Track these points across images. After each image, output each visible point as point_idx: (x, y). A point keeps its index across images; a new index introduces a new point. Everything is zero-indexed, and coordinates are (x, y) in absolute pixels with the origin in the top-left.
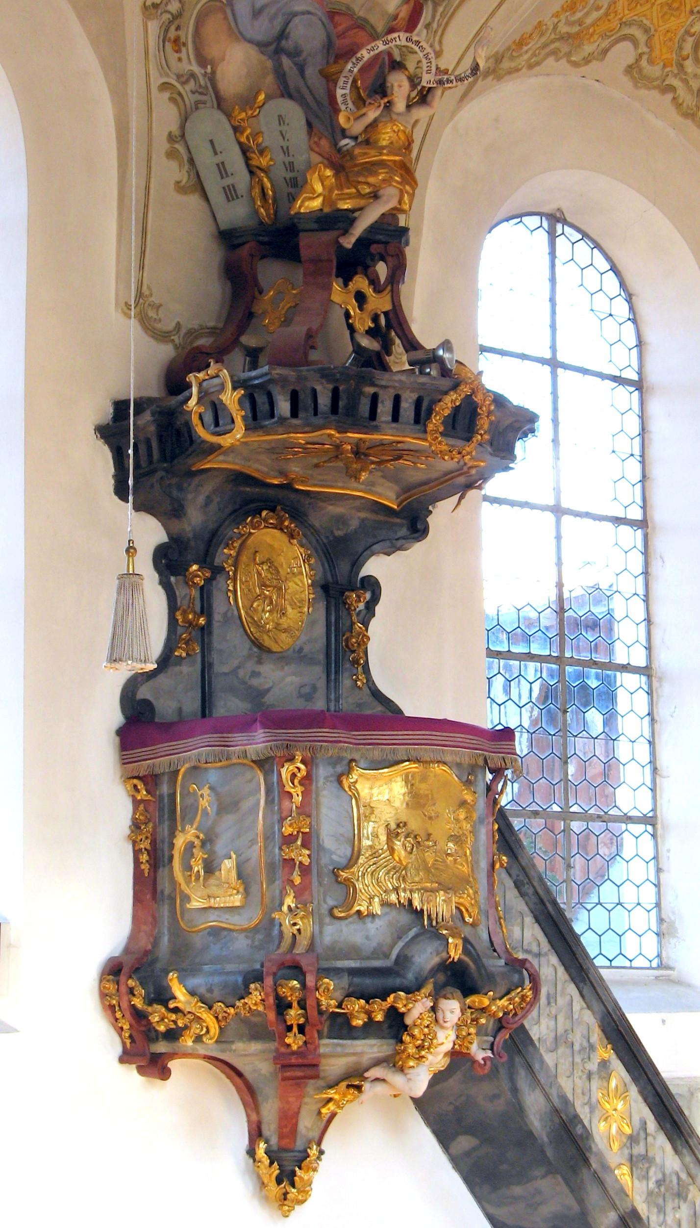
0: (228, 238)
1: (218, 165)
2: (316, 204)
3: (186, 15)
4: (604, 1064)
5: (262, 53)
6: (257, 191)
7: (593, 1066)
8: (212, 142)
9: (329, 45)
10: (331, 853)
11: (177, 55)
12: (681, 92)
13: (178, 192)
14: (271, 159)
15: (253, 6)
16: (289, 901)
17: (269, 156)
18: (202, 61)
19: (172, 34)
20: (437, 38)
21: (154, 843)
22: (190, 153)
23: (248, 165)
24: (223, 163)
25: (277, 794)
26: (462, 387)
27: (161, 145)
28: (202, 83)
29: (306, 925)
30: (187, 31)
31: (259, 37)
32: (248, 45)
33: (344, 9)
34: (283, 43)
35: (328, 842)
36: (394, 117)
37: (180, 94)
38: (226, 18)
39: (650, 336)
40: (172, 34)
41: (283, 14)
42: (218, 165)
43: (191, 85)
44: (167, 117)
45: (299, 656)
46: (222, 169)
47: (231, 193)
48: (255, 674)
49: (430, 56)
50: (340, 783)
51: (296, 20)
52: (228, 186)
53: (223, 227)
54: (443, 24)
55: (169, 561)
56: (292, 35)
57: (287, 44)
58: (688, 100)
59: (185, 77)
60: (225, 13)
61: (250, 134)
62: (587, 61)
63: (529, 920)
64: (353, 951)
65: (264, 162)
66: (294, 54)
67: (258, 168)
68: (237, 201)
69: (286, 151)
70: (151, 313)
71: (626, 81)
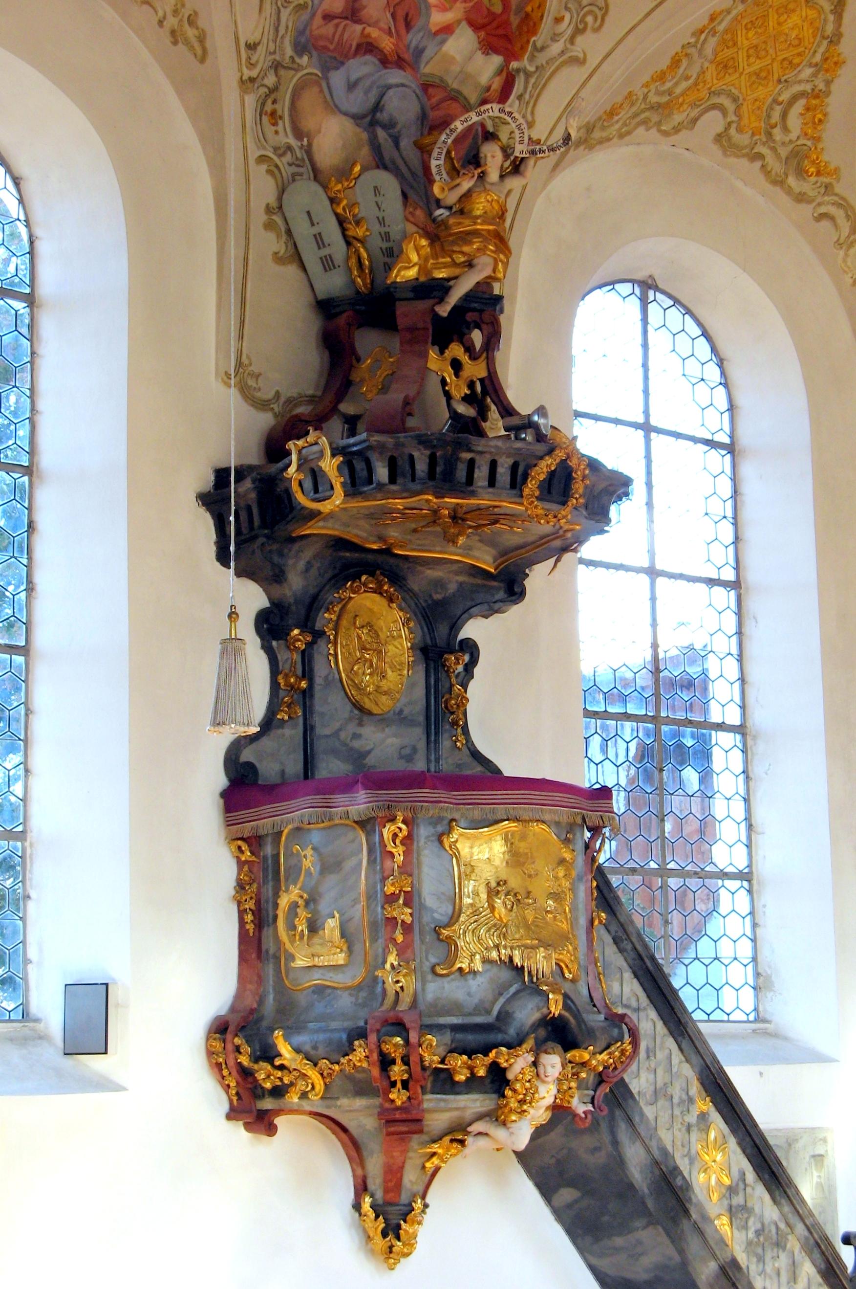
0: (325, 307)
1: (315, 236)
2: (412, 273)
3: (282, 88)
4: (703, 1116)
5: (357, 125)
6: (353, 262)
7: (692, 1118)
8: (308, 213)
9: (423, 117)
10: (432, 911)
11: (274, 128)
12: (770, 159)
14: (367, 230)
16: (392, 959)
18: (298, 133)
19: (269, 107)
20: (529, 109)
21: (258, 903)
22: (287, 224)
23: (345, 236)
24: (320, 234)
25: (379, 853)
27: (259, 217)
28: (299, 155)
29: (409, 983)
30: (284, 104)
31: (354, 110)
32: (344, 118)
33: (437, 81)
34: (378, 114)
35: (430, 901)
37: (277, 166)
38: (321, 91)
39: (741, 400)
40: (269, 107)
41: (378, 87)
42: (315, 236)
43: (288, 157)
44: (265, 189)
45: (399, 718)
47: (328, 264)
48: (356, 736)
49: (522, 127)
50: (441, 842)
51: (391, 92)
53: (321, 296)
55: (271, 625)
56: (386, 107)
57: (382, 116)
58: (776, 166)
59: (282, 150)
60: (320, 86)
61: (347, 205)
62: (677, 130)
63: (628, 975)
64: (455, 1008)
65: (360, 232)
66: (389, 126)
68: (334, 271)
69: (382, 222)
70: (251, 382)
71: (715, 149)
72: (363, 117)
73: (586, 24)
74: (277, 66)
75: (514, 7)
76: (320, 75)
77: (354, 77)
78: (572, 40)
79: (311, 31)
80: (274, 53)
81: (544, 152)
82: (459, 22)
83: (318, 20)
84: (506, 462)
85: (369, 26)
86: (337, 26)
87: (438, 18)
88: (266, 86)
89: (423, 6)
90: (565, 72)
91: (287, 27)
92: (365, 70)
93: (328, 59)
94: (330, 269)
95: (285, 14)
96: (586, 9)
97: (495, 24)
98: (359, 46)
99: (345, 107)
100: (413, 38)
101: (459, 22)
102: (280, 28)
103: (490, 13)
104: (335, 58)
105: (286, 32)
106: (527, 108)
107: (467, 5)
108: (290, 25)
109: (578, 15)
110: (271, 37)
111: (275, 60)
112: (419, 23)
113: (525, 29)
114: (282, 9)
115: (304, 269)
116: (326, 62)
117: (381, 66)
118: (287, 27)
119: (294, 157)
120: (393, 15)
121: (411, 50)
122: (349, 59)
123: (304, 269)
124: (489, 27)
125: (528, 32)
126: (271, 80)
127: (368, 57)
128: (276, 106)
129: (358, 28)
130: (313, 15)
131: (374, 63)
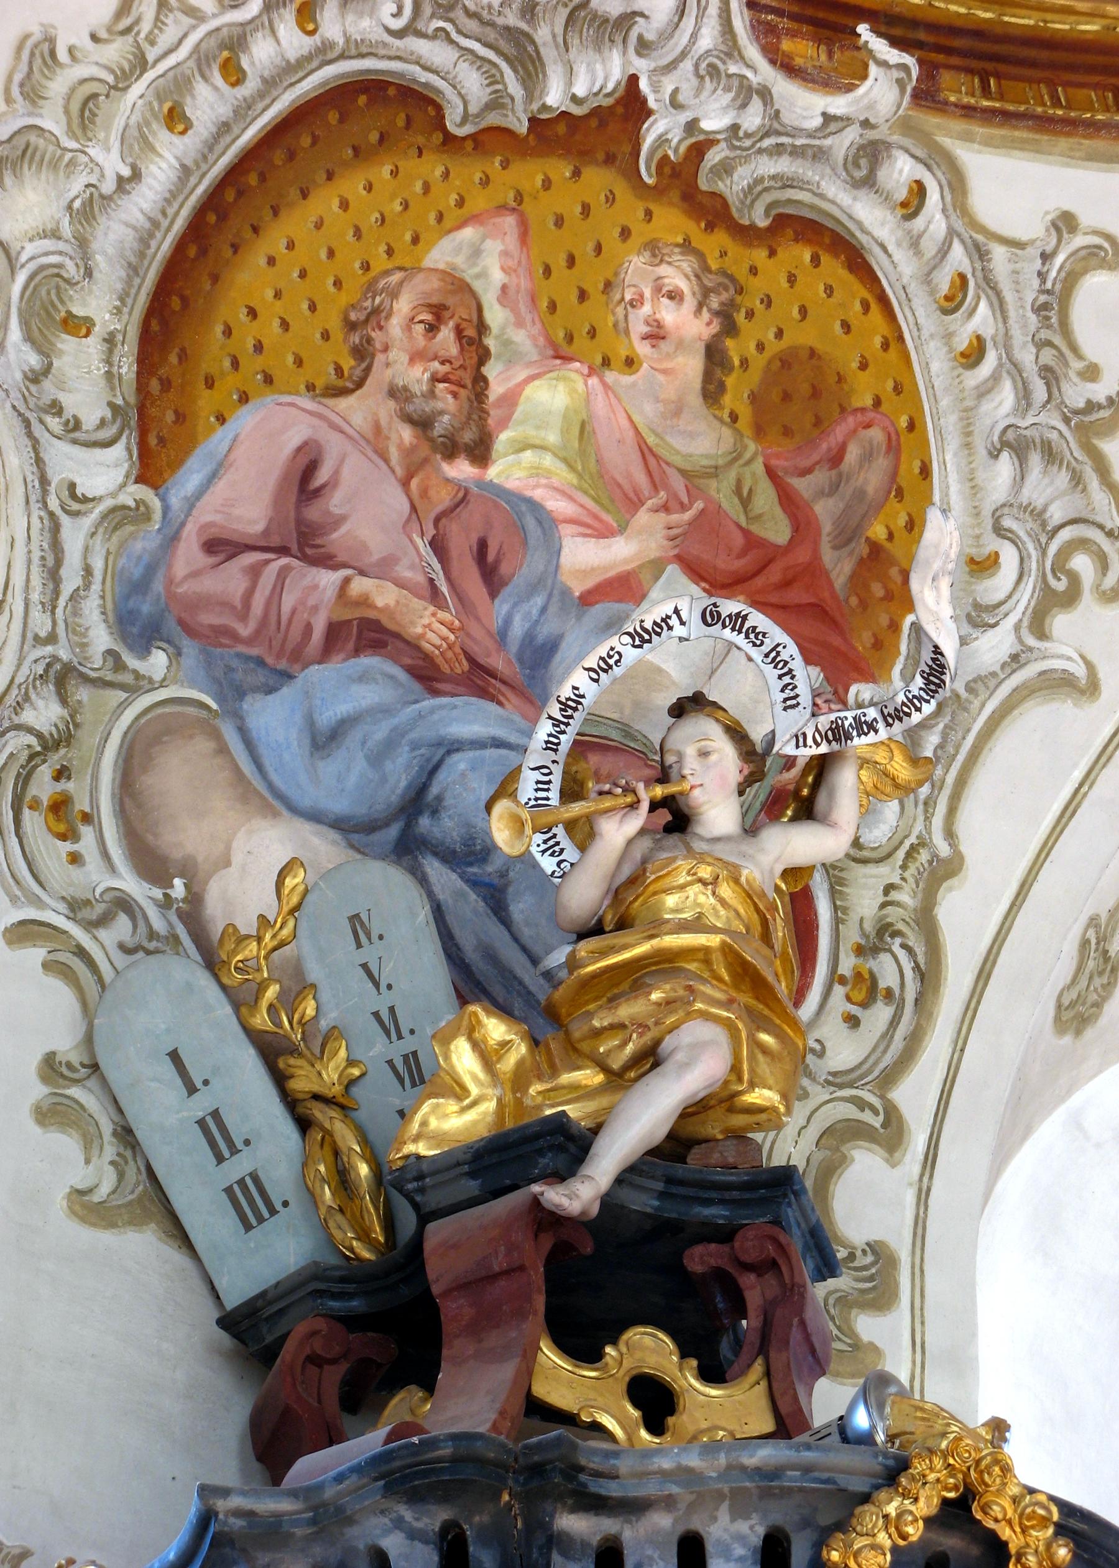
0: (250, 1330)
1: (201, 1123)
3: (88, 738)
5: (352, 846)
8: (175, 1056)
11: (67, 847)
13: (83, 1220)
14: (351, 1063)
15: (310, 722)
17: (343, 1053)
18: (152, 864)
19: (43, 787)
20: (938, 821)
22: (120, 1111)
23: (291, 1102)
24: (216, 1114)
26: (919, 1466)
28: (158, 924)
30: (95, 777)
31: (339, 806)
32: (307, 829)
33: (614, 735)
34: (424, 822)
36: (698, 846)
37: (81, 952)
38: (223, 749)
40: (43, 787)
41: (415, 746)
42: (201, 1123)
46: (217, 1137)
47: (250, 1203)
49: (784, 655)
51: (460, 762)
52: (241, 1182)
53: (232, 1300)
54: (950, 779)
56: (449, 801)
59: (100, 908)
60: (216, 735)
61: (280, 996)
65: (331, 1074)
67: (316, 1097)
68: (270, 1223)
69: (389, 1024)
72: (370, 827)
73: (1074, 580)
74: (62, 678)
75: (827, 527)
76: (214, 706)
77: (328, 716)
78: (1038, 624)
79: (170, 582)
80: (52, 639)
81: (872, 727)
82: (657, 567)
83: (188, 554)
84: (741, 1538)
85: (362, 573)
86: (255, 572)
87: (584, 557)
88: (30, 730)
89: (530, 523)
90: (1038, 719)
91: (88, 571)
92: (366, 696)
93: (235, 663)
94: (261, 1220)
95: (75, 535)
96: (1065, 534)
97: (775, 574)
98: (335, 634)
99: (309, 796)
100: (515, 614)
101: (657, 567)
102: (64, 572)
103: (752, 542)
104: (260, 662)
105: (87, 586)
106: (928, 819)
107: (675, 518)
108: (98, 565)
109: (1044, 552)
110: (35, 597)
111: (55, 658)
112: (532, 565)
113: (878, 590)
114: (65, 520)
115: (179, 1234)
116: (229, 669)
117: (417, 686)
118: (88, 571)
119: (142, 928)
120: (438, 546)
121: (513, 647)
122: (305, 666)
123: (179, 1234)
124: (759, 582)
125: (889, 597)
126: (45, 713)
127: (369, 661)
128: (70, 786)
129: (328, 580)
130: (172, 540)
131: (392, 677)
